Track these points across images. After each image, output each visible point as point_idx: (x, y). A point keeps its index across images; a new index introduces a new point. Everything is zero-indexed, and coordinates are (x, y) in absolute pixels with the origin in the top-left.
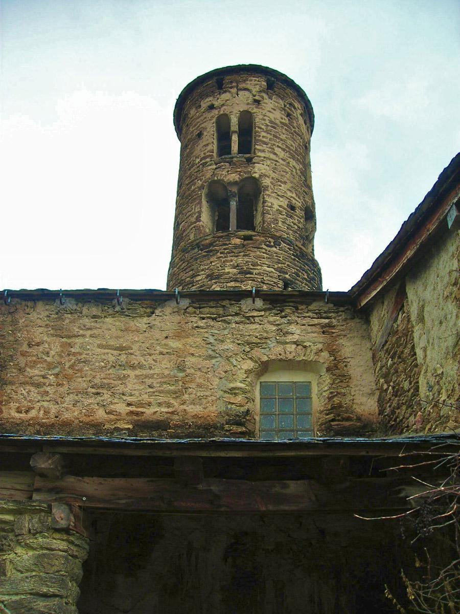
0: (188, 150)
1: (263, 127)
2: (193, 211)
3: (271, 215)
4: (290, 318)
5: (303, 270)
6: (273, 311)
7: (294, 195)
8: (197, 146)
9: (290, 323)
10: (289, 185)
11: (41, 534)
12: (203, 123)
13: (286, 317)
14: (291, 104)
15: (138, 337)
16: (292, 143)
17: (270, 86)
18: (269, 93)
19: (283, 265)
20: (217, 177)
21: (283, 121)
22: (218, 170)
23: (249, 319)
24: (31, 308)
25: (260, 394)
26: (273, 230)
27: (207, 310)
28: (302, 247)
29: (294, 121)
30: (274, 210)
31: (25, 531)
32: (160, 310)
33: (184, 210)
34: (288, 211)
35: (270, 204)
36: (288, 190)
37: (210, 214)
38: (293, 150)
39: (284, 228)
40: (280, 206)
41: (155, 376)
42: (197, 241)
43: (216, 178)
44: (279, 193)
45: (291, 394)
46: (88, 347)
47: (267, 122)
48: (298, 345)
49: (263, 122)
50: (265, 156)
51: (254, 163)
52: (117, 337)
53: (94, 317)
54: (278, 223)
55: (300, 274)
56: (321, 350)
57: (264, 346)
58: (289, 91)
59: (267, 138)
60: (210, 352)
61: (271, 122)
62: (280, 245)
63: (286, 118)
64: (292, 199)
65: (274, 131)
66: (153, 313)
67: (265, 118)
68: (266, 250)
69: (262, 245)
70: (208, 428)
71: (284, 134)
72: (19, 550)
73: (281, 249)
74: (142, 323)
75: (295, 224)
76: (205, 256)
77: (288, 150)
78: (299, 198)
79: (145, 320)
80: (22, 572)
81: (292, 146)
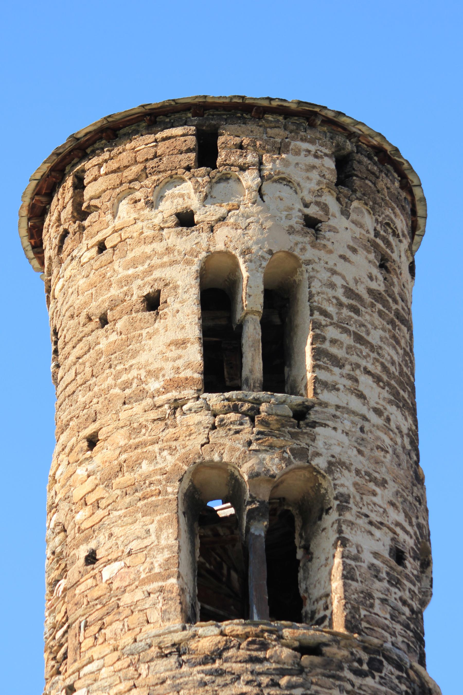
1: (331, 309)
3: (357, 581)
7: (401, 518)
12: (163, 265)
17: (344, 172)
21: (374, 285)
22: (221, 432)
30: (365, 565)
34: (391, 567)
35: (354, 551)
37: (189, 536)
38: (394, 378)
40: (376, 555)
43: (216, 458)
44: (374, 517)
47: (340, 293)
49: (331, 293)
51: (314, 424)
54: (372, 606)
61: (349, 292)
62: (381, 672)
64: (398, 530)
65: (356, 321)
75: (404, 603)
77: (385, 378)
81: (393, 363)
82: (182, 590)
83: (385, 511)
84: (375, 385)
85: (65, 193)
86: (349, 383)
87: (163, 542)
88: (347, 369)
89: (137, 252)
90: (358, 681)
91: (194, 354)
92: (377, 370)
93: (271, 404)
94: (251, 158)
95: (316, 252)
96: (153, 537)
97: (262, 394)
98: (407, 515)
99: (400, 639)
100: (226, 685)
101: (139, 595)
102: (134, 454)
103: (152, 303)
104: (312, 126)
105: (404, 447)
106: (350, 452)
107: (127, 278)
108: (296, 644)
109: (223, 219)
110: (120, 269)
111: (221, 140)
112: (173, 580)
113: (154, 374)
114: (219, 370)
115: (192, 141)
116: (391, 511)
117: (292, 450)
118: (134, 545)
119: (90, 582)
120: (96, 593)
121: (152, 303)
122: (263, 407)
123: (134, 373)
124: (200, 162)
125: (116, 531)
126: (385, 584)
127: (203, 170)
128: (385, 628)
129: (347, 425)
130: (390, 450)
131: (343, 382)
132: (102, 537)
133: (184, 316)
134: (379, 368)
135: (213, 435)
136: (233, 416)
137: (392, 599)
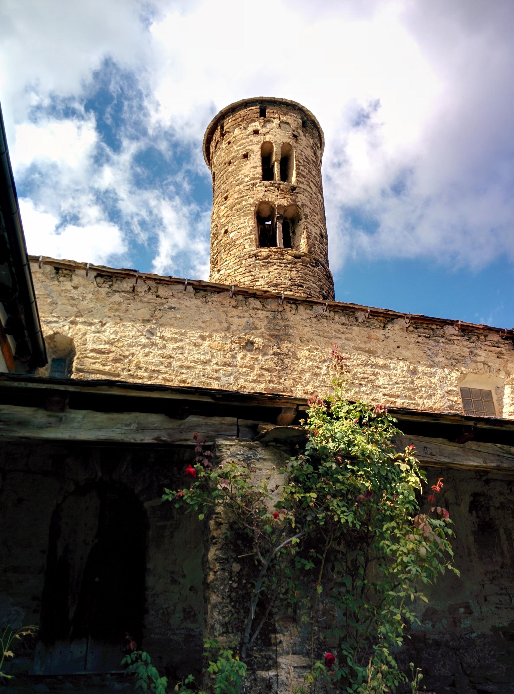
1: (301, 161)
8: (245, 165)
9: (476, 348)
17: (304, 124)
22: (268, 192)
40: (316, 233)
47: (304, 157)
51: (297, 193)
57: (464, 362)
61: (306, 158)
70: (441, 416)
74: (380, 333)
82: (256, 239)
85: (218, 132)
87: (250, 225)
88: (306, 179)
89: (241, 142)
90: (312, 268)
91: (260, 170)
93: (283, 185)
94: (276, 116)
97: (281, 182)
101: (242, 240)
102: (240, 200)
103: (246, 156)
104: (295, 109)
107: (237, 150)
109: (268, 132)
110: (235, 148)
111: (267, 111)
112: (253, 236)
113: (247, 176)
114: (267, 174)
115: (258, 110)
118: (240, 226)
119: (226, 239)
120: (228, 242)
121: (246, 156)
122: (281, 186)
123: (240, 176)
124: (261, 116)
125: (234, 223)
127: (262, 118)
132: (230, 225)
133: (256, 159)
135: (266, 193)
136: (272, 188)
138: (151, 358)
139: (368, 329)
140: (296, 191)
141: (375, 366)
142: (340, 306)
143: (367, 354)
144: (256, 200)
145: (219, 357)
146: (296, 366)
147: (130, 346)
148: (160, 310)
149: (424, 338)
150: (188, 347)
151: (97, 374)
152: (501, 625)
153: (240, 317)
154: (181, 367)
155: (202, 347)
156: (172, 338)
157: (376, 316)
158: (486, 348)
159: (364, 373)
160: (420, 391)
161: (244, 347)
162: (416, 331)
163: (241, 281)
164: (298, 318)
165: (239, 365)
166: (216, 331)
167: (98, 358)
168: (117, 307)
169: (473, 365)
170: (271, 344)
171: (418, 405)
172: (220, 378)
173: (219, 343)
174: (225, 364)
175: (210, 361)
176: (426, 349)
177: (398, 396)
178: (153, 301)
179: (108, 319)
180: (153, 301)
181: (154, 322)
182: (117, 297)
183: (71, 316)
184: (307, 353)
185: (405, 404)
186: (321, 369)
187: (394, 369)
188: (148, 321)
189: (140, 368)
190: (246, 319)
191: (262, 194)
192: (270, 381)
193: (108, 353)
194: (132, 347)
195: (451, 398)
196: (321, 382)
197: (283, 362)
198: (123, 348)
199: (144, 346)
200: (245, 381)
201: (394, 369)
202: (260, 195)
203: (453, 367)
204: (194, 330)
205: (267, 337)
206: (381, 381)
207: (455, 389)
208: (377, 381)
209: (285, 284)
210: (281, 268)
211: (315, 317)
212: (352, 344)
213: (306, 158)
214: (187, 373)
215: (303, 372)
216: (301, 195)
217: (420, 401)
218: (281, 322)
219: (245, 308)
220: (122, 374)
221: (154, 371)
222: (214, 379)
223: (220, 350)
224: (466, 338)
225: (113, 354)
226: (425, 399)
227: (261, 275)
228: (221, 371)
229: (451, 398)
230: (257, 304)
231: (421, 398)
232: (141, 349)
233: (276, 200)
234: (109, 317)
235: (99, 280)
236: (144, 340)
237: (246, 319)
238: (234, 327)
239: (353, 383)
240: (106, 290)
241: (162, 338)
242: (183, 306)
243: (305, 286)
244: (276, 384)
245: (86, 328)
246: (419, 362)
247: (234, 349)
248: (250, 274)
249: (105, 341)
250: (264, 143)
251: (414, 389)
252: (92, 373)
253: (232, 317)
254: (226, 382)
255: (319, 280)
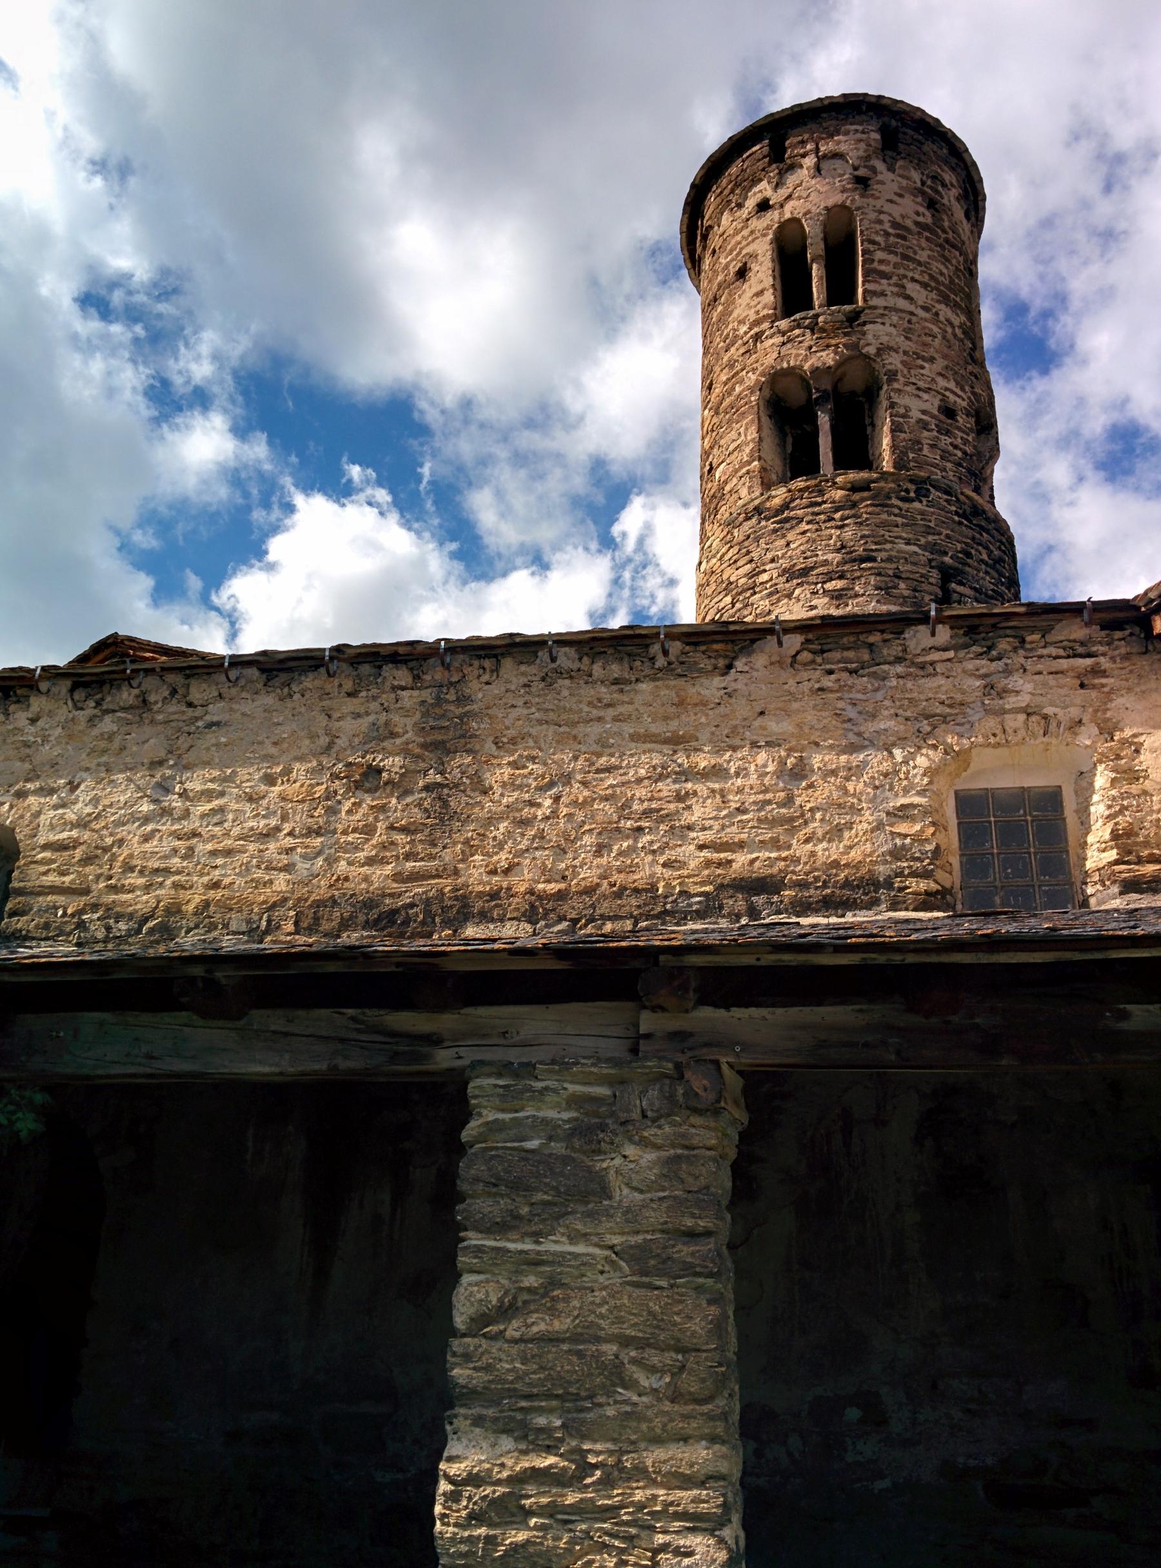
0: (720, 308)
1: (878, 239)
2: (743, 437)
4: (1009, 661)
5: (980, 544)
6: (974, 648)
7: (952, 385)
8: (740, 297)
9: (1008, 672)
10: (940, 363)
11: (669, 1119)
12: (748, 244)
13: (1000, 659)
14: (934, 178)
15: (707, 715)
16: (942, 267)
18: (888, 159)
19: (936, 537)
20: (788, 362)
21: (921, 219)
22: (789, 346)
23: (926, 669)
24: (492, 671)
25: (958, 817)
26: (912, 464)
27: (837, 655)
28: (973, 495)
29: (945, 217)
30: (913, 421)
31: (636, 1115)
32: (744, 660)
33: (721, 438)
34: (940, 421)
35: (902, 411)
36: (940, 374)
38: (943, 284)
39: (934, 457)
40: (924, 412)
41: (747, 790)
42: (756, 502)
43: (785, 365)
44: (921, 384)
45: (1022, 812)
46: (611, 741)
48: (1029, 715)
49: (878, 227)
50: (885, 304)
51: (864, 324)
52: (666, 718)
53: (616, 682)
54: (921, 450)
55: (973, 552)
56: (1080, 721)
57: (960, 719)
58: (929, 147)
59: (887, 263)
60: (852, 737)
61: (895, 225)
63: (927, 213)
64: (947, 393)
65: (902, 245)
66: (730, 667)
67: (882, 217)
68: (901, 509)
69: (890, 498)
71: (923, 249)
72: (630, 1150)
73: (931, 504)
74: (711, 688)
75: (956, 447)
76: (775, 531)
77: (933, 284)
78: (963, 389)
79: (717, 681)
80: (641, 1192)
81: (942, 274)
83: (933, 379)
84: (922, 290)
86: (895, 289)
87: (749, 438)
88: (895, 279)
89: (733, 242)
90: (905, 506)
92: (926, 278)
95: (865, 200)
96: (743, 437)
98: (957, 383)
99: (951, 473)
100: (792, 528)
101: (735, 480)
102: (730, 384)
103: (742, 273)
105: (955, 335)
106: (897, 339)
108: (849, 485)
113: (742, 322)
114: (792, 295)
116: (939, 380)
117: (844, 345)
121: (742, 273)
126: (935, 433)
128: (936, 466)
129: (895, 319)
130: (939, 336)
131: (889, 290)
133: (763, 274)
134: (927, 277)
135: (784, 350)
136: (797, 332)
137: (942, 445)
138: (155, 843)
139: (681, 682)
140: (863, 318)
141: (685, 774)
142: (602, 639)
143: (667, 749)
144: (762, 374)
145: (298, 818)
146: (476, 810)
147: (120, 823)
148: (189, 734)
149: (845, 675)
150: (236, 807)
151: (48, 894)
152: (972, 1463)
153: (358, 716)
154: (214, 853)
155: (264, 802)
156: (203, 792)
157: (704, 643)
158: (1040, 667)
159: (650, 800)
160: (806, 823)
161: (358, 785)
162: (819, 660)
163: (732, 579)
164: (496, 689)
165: (340, 827)
166: (301, 759)
167: (53, 861)
168: (103, 744)
169: (991, 723)
170: (422, 765)
171: (798, 861)
172: (294, 865)
173: (302, 786)
174: (310, 832)
175: (278, 829)
176: (841, 704)
177: (741, 845)
178: (176, 717)
179: (84, 775)
180: (176, 717)
181: (171, 762)
182: (108, 724)
183: (17, 783)
184: (507, 771)
185: (757, 864)
186: (539, 805)
187: (737, 774)
188: (161, 763)
189: (132, 869)
190: (371, 718)
191: (775, 355)
192: (408, 857)
193: (75, 848)
194: (124, 824)
195: (902, 828)
196: (534, 837)
197: (445, 804)
198: (105, 832)
199: (146, 820)
200: (350, 864)
201: (737, 774)
202: (770, 360)
203: (922, 739)
204: (252, 764)
205: (417, 751)
206: (697, 813)
207: (917, 800)
208: (686, 813)
209: (826, 563)
210: (816, 526)
211: (543, 679)
212: (628, 729)
213: (895, 225)
214: (224, 866)
215: (491, 821)
216: (878, 327)
217: (801, 850)
218: (452, 708)
219: (374, 691)
220: (94, 887)
221: (157, 870)
222: (280, 870)
223: (303, 801)
224: (976, 649)
225: (83, 847)
226: (820, 841)
227: (769, 556)
228: (299, 850)
229: (902, 828)
230: (402, 676)
231: (807, 841)
232: (140, 826)
233: (806, 359)
234: (87, 769)
235: (79, 695)
236: (146, 807)
237: (371, 718)
238: (341, 742)
239: (618, 829)
240: (89, 712)
241: (184, 795)
242: (238, 715)
243: (880, 556)
244: (422, 859)
245: (42, 800)
246: (817, 744)
247: (335, 792)
248: (747, 558)
249: (71, 823)
250: (783, 226)
251: (792, 819)
252: (39, 894)
253: (339, 719)
254: (305, 873)
255: (928, 531)
